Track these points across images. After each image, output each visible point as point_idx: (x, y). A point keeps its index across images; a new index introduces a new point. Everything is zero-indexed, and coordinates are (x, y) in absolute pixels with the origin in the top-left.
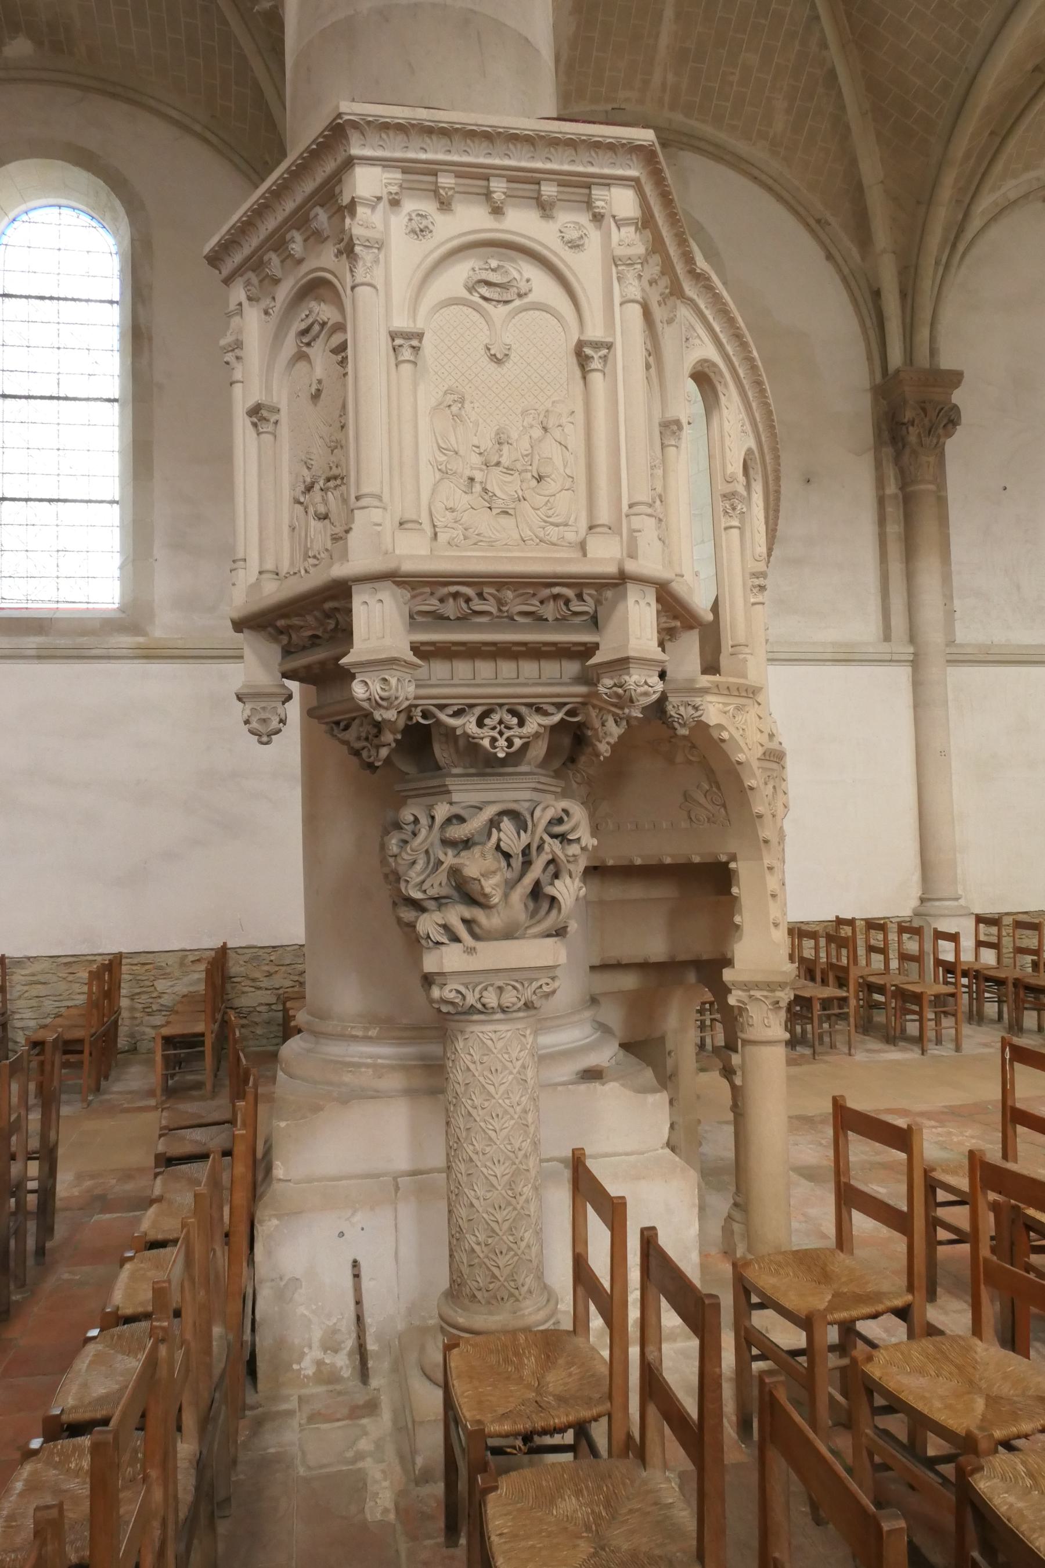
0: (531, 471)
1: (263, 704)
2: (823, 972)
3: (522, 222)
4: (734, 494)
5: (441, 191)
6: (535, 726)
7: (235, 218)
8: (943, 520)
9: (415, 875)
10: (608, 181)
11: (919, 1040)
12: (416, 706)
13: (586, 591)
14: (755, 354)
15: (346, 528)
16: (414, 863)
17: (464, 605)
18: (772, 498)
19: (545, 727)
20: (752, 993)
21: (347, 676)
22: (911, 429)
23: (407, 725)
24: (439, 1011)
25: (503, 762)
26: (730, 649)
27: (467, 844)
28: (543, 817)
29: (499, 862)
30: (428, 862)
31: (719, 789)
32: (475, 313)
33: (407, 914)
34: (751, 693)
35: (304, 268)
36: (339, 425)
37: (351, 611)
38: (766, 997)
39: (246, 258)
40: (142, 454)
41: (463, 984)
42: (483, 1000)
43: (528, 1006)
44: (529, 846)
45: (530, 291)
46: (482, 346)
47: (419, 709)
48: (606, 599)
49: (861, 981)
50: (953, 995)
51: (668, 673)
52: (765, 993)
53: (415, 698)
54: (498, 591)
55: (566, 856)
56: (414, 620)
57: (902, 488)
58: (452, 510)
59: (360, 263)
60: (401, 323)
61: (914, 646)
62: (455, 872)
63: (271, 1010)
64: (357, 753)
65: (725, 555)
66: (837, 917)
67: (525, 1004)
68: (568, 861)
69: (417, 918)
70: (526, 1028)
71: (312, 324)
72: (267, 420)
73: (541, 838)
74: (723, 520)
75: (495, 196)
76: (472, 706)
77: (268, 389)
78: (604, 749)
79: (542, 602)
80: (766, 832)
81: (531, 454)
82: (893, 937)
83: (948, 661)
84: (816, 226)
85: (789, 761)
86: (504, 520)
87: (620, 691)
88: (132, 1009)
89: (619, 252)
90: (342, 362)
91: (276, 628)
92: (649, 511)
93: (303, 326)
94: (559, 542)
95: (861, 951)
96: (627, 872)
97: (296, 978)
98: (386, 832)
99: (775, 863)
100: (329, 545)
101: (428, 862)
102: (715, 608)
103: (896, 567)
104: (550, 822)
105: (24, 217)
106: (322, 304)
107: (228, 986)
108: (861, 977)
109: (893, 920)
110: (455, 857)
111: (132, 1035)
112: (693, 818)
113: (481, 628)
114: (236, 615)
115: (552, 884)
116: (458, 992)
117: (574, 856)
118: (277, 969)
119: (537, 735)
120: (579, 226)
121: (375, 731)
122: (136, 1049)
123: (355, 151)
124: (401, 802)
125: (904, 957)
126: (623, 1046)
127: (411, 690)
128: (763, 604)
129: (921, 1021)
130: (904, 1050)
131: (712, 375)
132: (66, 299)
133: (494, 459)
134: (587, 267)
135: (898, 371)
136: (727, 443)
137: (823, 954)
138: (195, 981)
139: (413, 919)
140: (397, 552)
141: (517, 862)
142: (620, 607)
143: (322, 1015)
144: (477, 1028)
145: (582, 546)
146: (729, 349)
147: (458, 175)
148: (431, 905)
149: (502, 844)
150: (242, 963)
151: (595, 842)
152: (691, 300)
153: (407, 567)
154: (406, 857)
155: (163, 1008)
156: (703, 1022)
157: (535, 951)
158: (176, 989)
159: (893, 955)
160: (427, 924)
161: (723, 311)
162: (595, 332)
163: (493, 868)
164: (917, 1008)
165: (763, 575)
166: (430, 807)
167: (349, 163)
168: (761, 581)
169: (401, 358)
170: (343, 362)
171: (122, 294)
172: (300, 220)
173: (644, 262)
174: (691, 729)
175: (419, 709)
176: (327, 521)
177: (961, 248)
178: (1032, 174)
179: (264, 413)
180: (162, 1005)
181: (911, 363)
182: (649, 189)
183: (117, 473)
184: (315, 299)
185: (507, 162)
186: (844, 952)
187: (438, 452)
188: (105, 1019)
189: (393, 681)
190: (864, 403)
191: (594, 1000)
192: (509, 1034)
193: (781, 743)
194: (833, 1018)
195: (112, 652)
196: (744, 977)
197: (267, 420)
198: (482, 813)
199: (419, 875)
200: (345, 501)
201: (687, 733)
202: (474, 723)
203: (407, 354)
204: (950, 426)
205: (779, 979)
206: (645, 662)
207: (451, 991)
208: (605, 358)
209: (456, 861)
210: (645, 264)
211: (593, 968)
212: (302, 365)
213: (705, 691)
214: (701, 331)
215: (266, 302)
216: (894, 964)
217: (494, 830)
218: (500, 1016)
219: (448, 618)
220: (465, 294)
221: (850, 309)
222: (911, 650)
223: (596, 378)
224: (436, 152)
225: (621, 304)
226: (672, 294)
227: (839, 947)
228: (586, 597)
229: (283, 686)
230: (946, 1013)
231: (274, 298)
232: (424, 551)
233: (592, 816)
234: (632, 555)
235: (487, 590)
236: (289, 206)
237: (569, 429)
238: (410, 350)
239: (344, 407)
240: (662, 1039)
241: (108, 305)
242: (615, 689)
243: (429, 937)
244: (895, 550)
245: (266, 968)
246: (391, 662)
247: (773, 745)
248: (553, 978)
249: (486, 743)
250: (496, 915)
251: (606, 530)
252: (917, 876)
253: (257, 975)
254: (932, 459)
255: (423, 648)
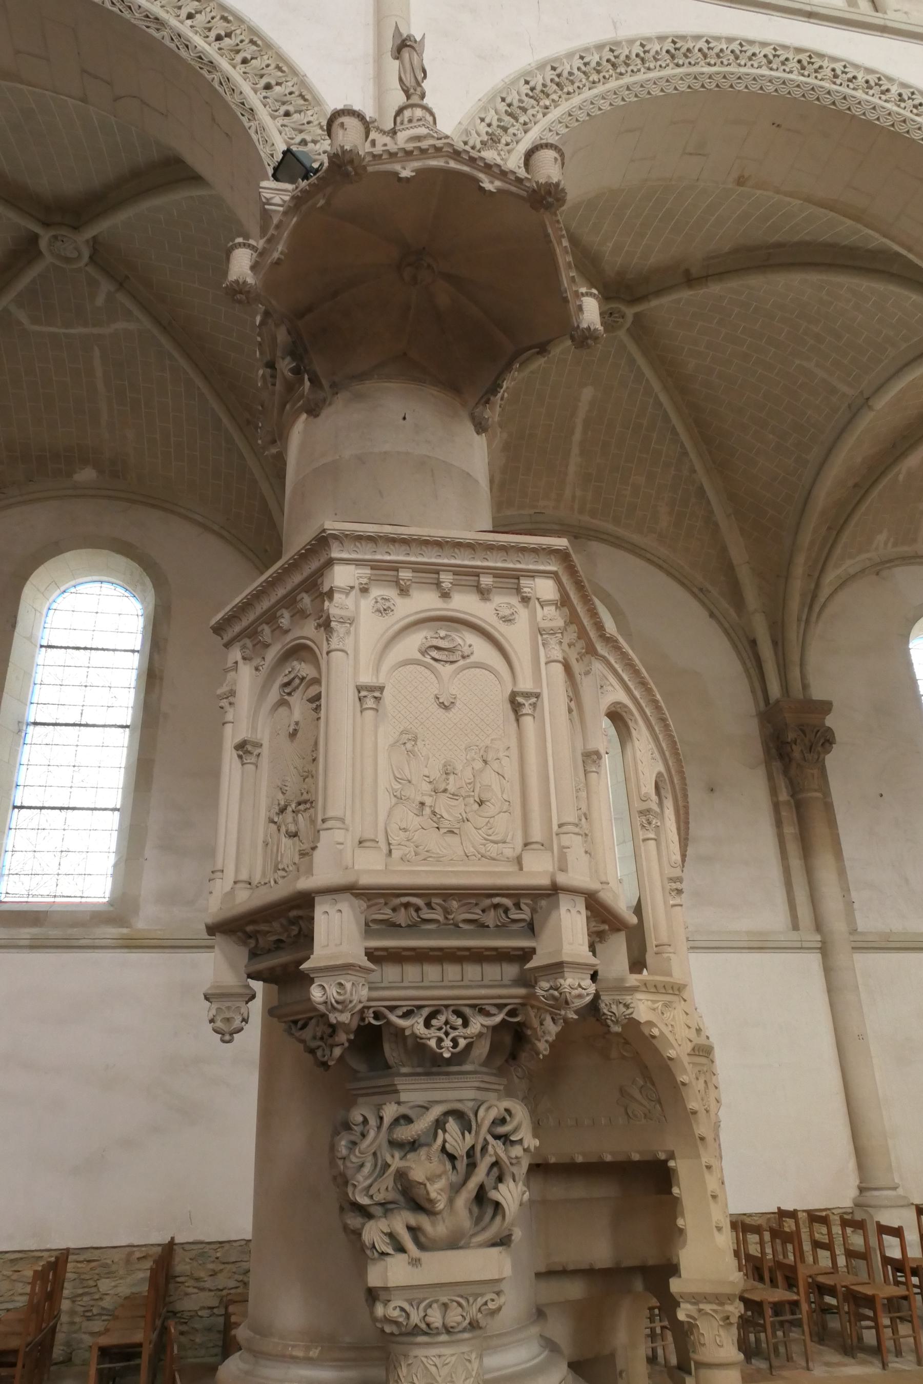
0: (474, 796)
1: (229, 1004)
2: (770, 1270)
3: (465, 603)
4: (649, 810)
5: (401, 582)
6: (479, 1026)
7: (237, 600)
8: (832, 823)
9: (362, 1179)
10: (533, 574)
11: (878, 1351)
12: (369, 1008)
13: (523, 901)
14: (658, 697)
15: (312, 845)
16: (362, 1165)
17: (414, 914)
18: (682, 812)
19: (487, 1027)
20: (702, 1306)
21: (306, 979)
22: (794, 746)
23: (359, 1026)
24: (383, 1331)
25: (449, 1062)
26: (655, 949)
27: (413, 1146)
28: (487, 1116)
29: (445, 1165)
30: (376, 1165)
31: (653, 1084)
32: (426, 670)
33: (354, 1221)
34: (677, 990)
35: (289, 637)
36: (311, 758)
37: (313, 919)
38: (714, 1311)
39: (243, 629)
40: (144, 771)
41: (407, 1300)
42: (428, 1319)
43: (474, 1326)
44: (473, 1147)
45: (472, 653)
46: (433, 696)
47: (371, 1010)
48: (541, 908)
49: (810, 1280)
50: (905, 1298)
51: (600, 973)
52: (715, 1307)
53: (369, 1000)
54: (444, 901)
55: (509, 1158)
56: (370, 928)
57: (792, 796)
58: (405, 830)
59: (335, 635)
60: (366, 678)
61: (822, 936)
62: (401, 1175)
63: (212, 1315)
64: (312, 1051)
65: (644, 863)
66: (779, 1208)
67: (470, 1324)
68: (511, 1164)
69: (363, 1225)
70: (471, 1352)
71: (294, 679)
72: (250, 753)
73: (485, 1139)
74: (641, 833)
75: (443, 585)
76: (420, 1007)
77: (254, 729)
78: (543, 1047)
79: (483, 911)
80: (701, 1129)
81: (474, 782)
82: (837, 1230)
83: (853, 948)
84: (699, 594)
85: (718, 1054)
86: (450, 838)
87: (556, 993)
88: (72, 1313)
89: (543, 624)
90: (316, 709)
91: (245, 932)
92: (576, 830)
93: (286, 680)
94: (498, 857)
95: (807, 1247)
96: (569, 1170)
97: (240, 1278)
98: (336, 1133)
99: (713, 1162)
100: (296, 859)
101: (376, 1165)
102: (638, 910)
103: (796, 863)
104: (493, 1122)
105: (73, 590)
106: (303, 664)
107: (172, 1286)
108: (810, 1277)
109: (835, 1212)
110: (401, 1159)
111: (68, 1344)
112: (631, 1115)
113: (428, 934)
114: (209, 921)
115: (496, 1188)
116: (402, 1309)
117: (517, 1158)
118: (222, 1267)
119: (480, 1035)
120: (511, 606)
121: (330, 1030)
122: (70, 1360)
123: (335, 555)
124: (350, 1102)
125: (850, 1254)
126: (572, 1366)
127: (364, 993)
128: (681, 905)
129: (877, 1327)
130: (863, 1363)
131: (624, 714)
132: (97, 649)
133: (442, 787)
134: (518, 636)
135: (778, 702)
136: (640, 768)
137: (769, 1250)
138: (137, 1281)
139: (359, 1226)
140: (356, 867)
141: (462, 1165)
142: (554, 915)
143: (262, 1331)
144: (420, 1352)
145: (519, 861)
146: (637, 694)
147: (414, 571)
148: (377, 1211)
149: (447, 1146)
150: (188, 1260)
151: (537, 1142)
152: (604, 657)
153: (365, 880)
154: (354, 1159)
155: (104, 1312)
156: (653, 1330)
157: (480, 1263)
158: (119, 1290)
159: (839, 1251)
160: (373, 1233)
161: (630, 665)
162: (526, 684)
163: (438, 1172)
164: (871, 1314)
165: (680, 880)
166: (379, 1107)
167: (330, 563)
168: (678, 885)
169: (365, 706)
170: (317, 709)
171: (143, 645)
172: (290, 601)
173: (563, 631)
174: (623, 1026)
175: (371, 1010)
176: (296, 838)
177: (816, 609)
178: (864, 556)
179: (249, 748)
180: (103, 1309)
181: (788, 696)
182: (565, 579)
183: (121, 786)
184: (297, 660)
185: (453, 561)
186: (790, 1247)
187: (393, 781)
188: (44, 1325)
189: (348, 986)
190: (753, 727)
191: (540, 1314)
192: (454, 1358)
193: (708, 1038)
194: (786, 1325)
195: (97, 943)
196: (693, 1289)
197: (250, 753)
198: (429, 1113)
199: (366, 1178)
200: (313, 821)
201: (620, 1030)
202: (422, 1023)
203: (370, 703)
204: (827, 745)
205: (727, 1290)
206: (577, 966)
207: (395, 1308)
208: (534, 705)
209: (402, 1164)
210: (565, 633)
211: (538, 1275)
212: (283, 710)
213: (634, 990)
214: (612, 679)
215: (257, 661)
216: (842, 1261)
217: (440, 1131)
218: (444, 1338)
219: (400, 926)
220: (419, 656)
221: (733, 655)
222: (818, 938)
223: (528, 721)
224: (398, 555)
225: (546, 663)
226: (587, 653)
227: (784, 1243)
228: (523, 906)
229: (248, 987)
230: (902, 1319)
231: (264, 658)
232: (380, 867)
233: (533, 1113)
234: (563, 869)
235: (435, 900)
236: (281, 592)
237: (505, 761)
238: (372, 700)
239: (316, 744)
240: (612, 1356)
241: (131, 654)
242: (551, 991)
243: (374, 1247)
244: (793, 849)
245: (211, 1266)
246: (346, 968)
247: (702, 1041)
248: (498, 1293)
249: (433, 1043)
250: (441, 1223)
251: (540, 847)
252: (852, 1164)
253: (202, 1274)
254: (815, 772)
255: (376, 953)
